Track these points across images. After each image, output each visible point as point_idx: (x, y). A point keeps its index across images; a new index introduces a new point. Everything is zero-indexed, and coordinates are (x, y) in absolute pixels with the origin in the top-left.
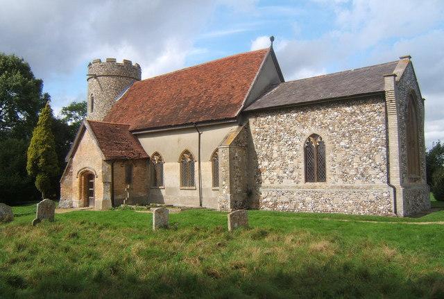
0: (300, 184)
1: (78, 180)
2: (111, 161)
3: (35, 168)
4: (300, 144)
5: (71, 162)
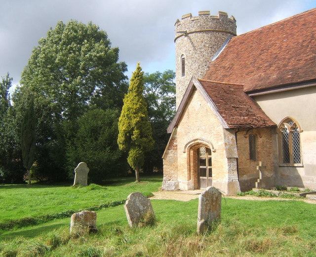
1: (185, 155)
2: (235, 130)
3: (128, 140)
5: (175, 133)
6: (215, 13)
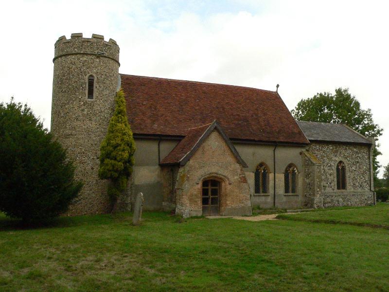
0: (335, 191)
4: (334, 166)
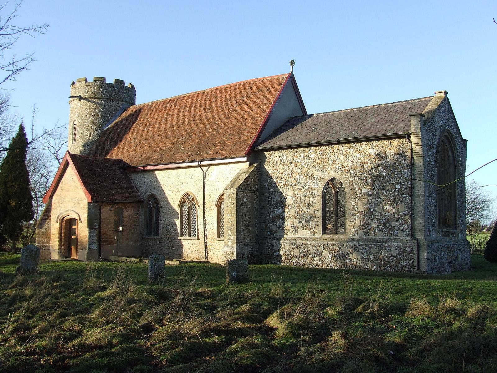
6: (110, 80)
